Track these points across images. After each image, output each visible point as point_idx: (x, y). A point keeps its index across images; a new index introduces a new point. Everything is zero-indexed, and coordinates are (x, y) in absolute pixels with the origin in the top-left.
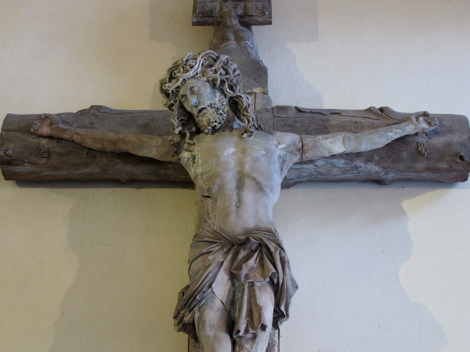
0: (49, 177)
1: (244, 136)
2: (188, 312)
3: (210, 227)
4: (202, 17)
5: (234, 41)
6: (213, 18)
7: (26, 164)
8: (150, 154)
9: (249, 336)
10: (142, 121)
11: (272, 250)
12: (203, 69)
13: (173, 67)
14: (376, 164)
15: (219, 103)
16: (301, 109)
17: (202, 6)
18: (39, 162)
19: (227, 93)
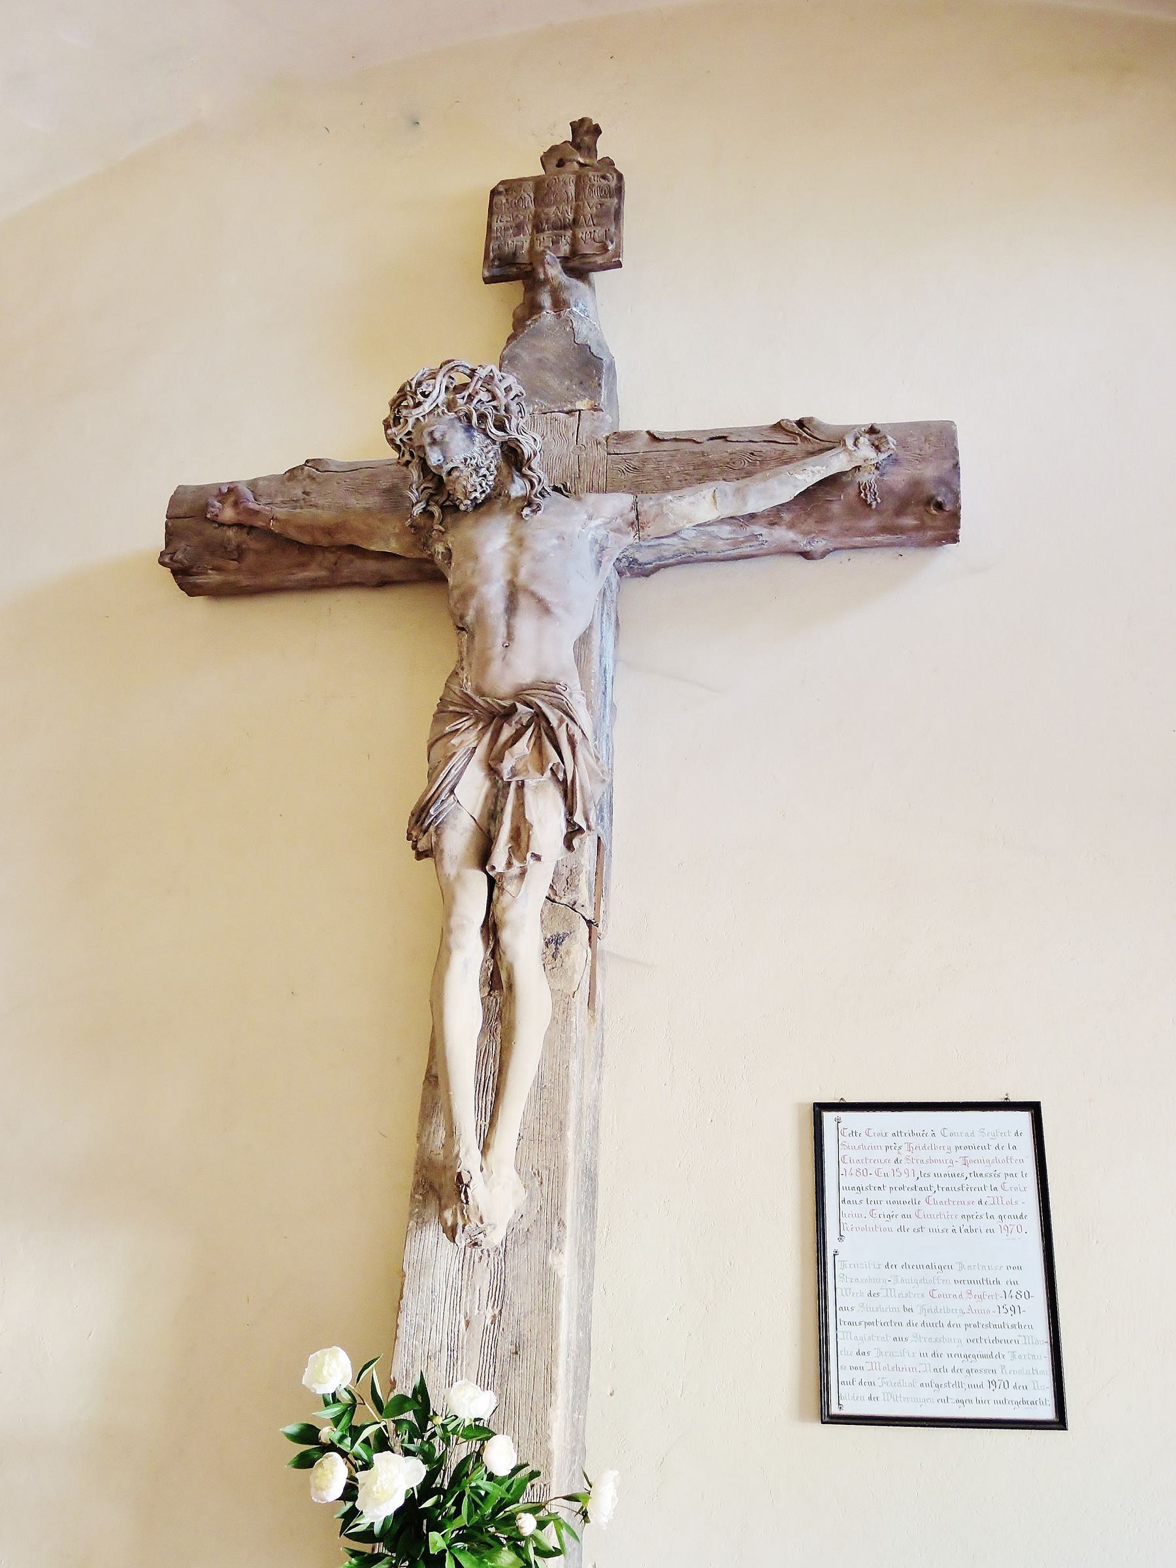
2: (422, 834)
7: (210, 571)
9: (515, 870)
11: (554, 723)
13: (399, 398)
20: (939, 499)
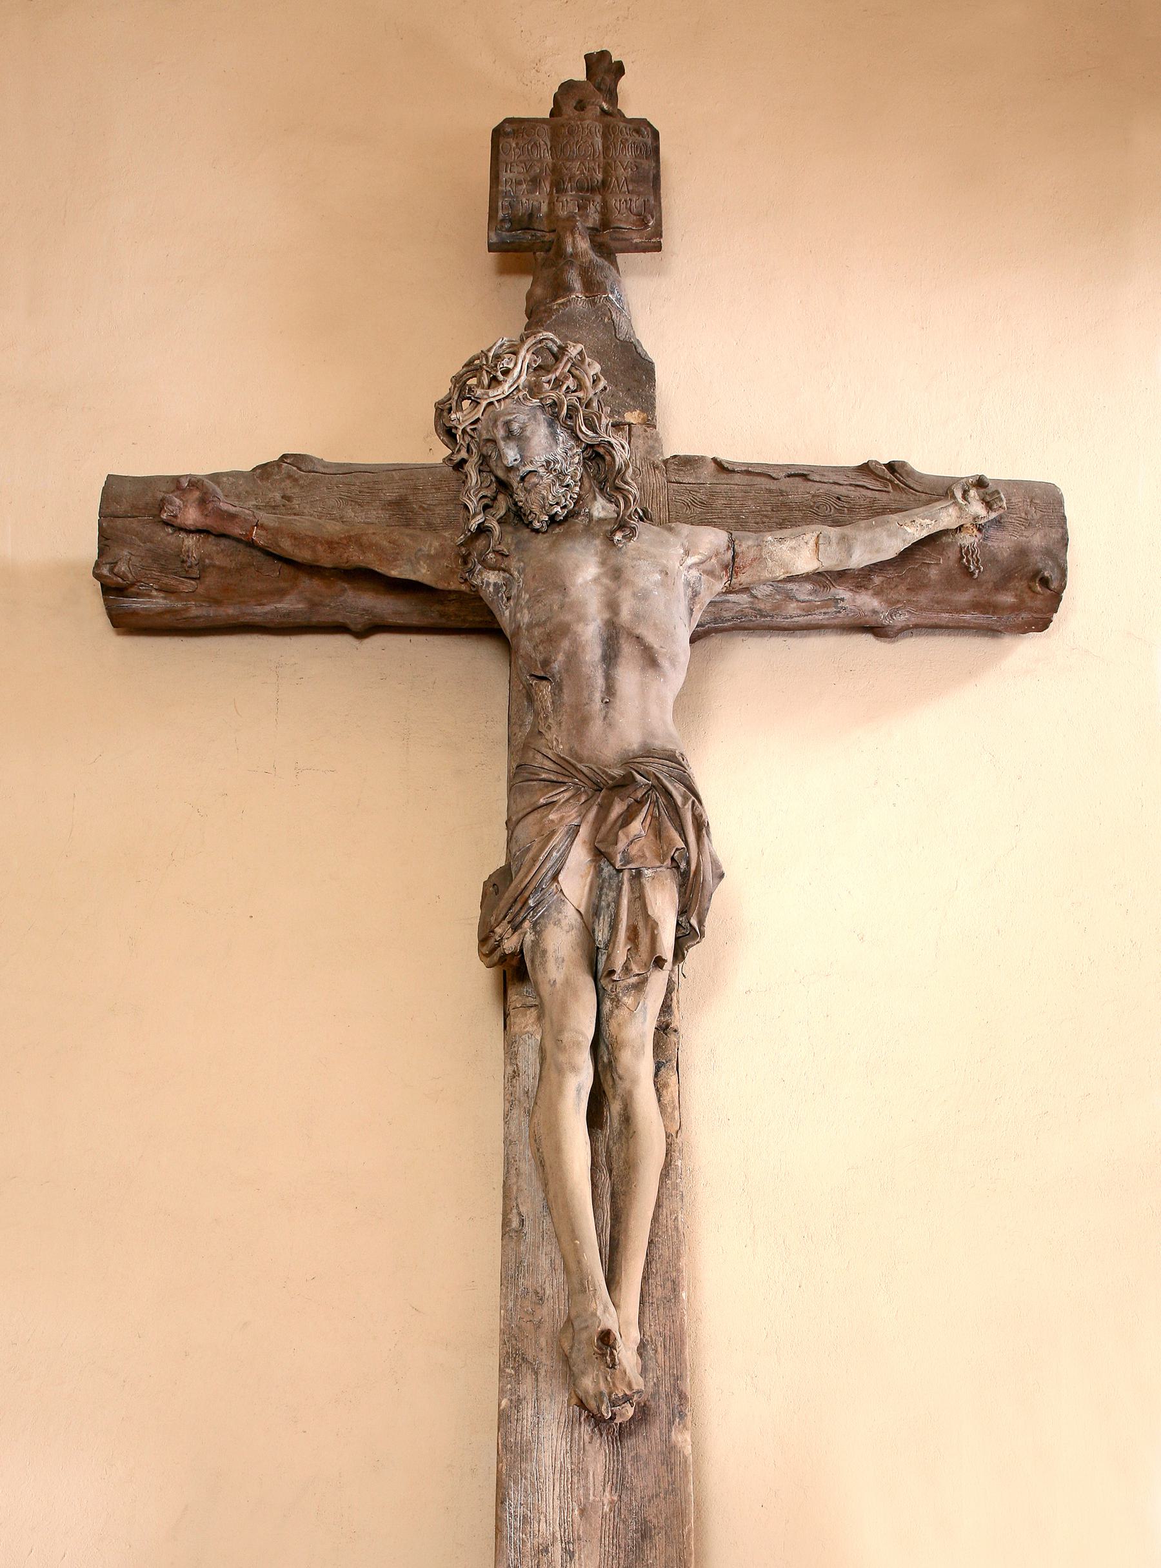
0: (202, 620)
1: (616, 538)
3: (550, 749)
4: (509, 230)
5: (582, 293)
6: (533, 232)
7: (154, 593)
8: (415, 573)
10: (392, 493)
11: (679, 800)
12: (529, 378)
14: (875, 594)
15: (564, 459)
16: (726, 465)
17: (510, 204)
18: (181, 587)
19: (580, 435)
20: (1046, 574)
